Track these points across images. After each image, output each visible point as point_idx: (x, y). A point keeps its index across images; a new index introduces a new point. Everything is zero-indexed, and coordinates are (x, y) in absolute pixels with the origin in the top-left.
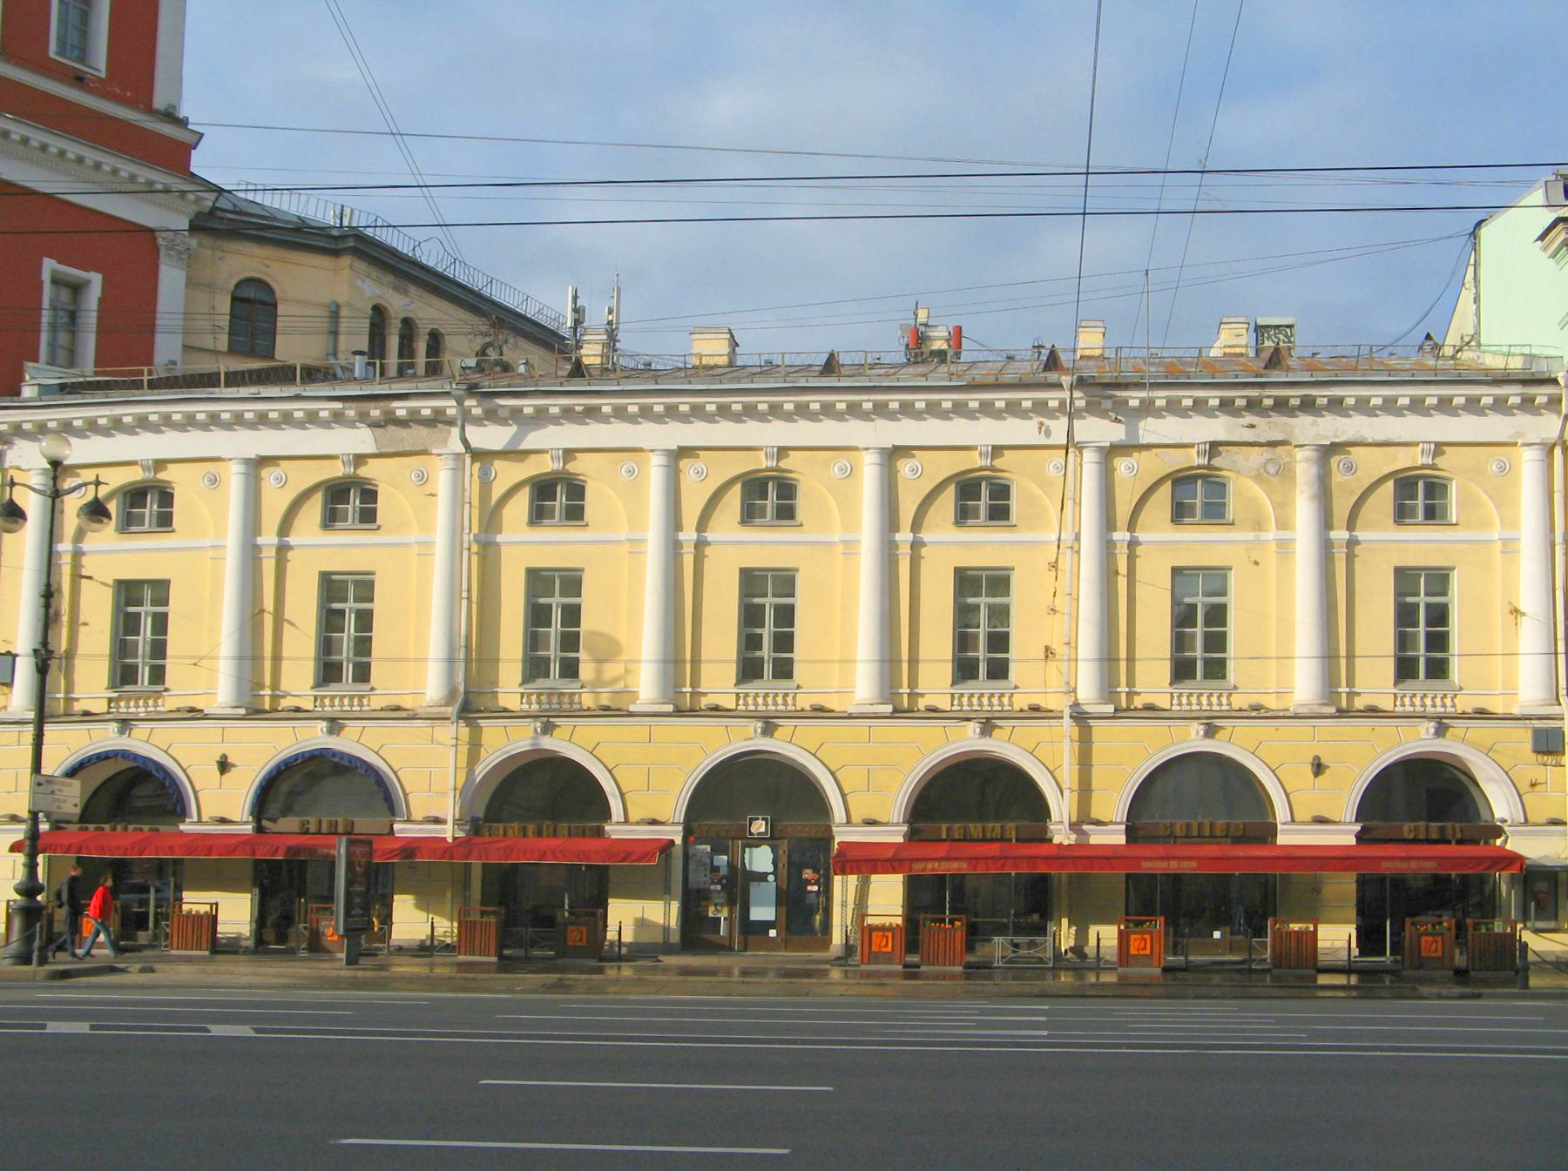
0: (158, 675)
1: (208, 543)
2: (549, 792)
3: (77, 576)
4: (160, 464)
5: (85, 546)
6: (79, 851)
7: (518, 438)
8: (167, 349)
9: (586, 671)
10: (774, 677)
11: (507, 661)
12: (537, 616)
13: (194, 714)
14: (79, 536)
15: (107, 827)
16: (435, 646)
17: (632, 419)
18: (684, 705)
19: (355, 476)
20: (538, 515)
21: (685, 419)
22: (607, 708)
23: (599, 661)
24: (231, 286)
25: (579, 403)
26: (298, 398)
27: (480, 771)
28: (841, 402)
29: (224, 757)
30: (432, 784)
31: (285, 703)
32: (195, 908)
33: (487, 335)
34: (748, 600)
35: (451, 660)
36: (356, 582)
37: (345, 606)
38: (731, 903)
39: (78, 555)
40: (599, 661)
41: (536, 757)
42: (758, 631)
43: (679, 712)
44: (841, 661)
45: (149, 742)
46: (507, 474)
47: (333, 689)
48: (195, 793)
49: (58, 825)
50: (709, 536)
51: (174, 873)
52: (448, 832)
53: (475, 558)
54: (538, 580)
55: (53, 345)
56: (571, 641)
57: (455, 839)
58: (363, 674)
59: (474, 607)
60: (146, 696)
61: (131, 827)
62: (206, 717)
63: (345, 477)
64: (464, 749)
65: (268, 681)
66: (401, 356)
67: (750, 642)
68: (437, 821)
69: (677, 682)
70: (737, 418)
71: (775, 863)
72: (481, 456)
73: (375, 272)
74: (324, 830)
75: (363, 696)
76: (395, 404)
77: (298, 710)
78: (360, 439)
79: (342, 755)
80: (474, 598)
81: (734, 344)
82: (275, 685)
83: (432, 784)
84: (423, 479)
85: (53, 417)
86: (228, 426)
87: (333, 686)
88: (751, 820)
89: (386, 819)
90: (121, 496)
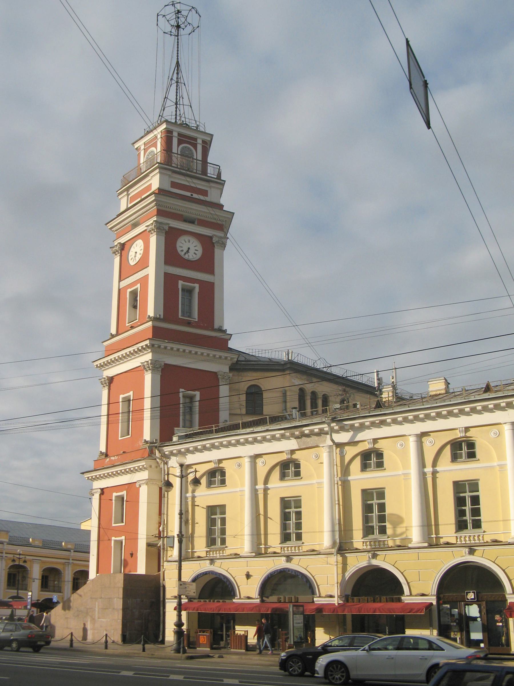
0: (223, 541)
1: (238, 489)
2: (376, 583)
3: (194, 506)
4: (220, 461)
5: (196, 494)
6: (197, 610)
7: (354, 436)
8: (224, 416)
9: (389, 531)
10: (473, 528)
11: (359, 530)
12: (367, 509)
13: (237, 556)
14: (193, 491)
15: (207, 600)
16: (326, 526)
17: (400, 423)
18: (433, 542)
19: (291, 458)
20: (365, 467)
21: (422, 420)
22: (399, 546)
23: (394, 528)
24: (245, 389)
25: (377, 419)
26: (267, 431)
27: (348, 575)
28: (491, 404)
29: (248, 572)
30: (329, 582)
31: (270, 550)
32: (239, 633)
33: (342, 395)
34: (458, 495)
35: (333, 531)
36: (294, 500)
37: (291, 509)
38: (461, 631)
39: (193, 497)
40: (394, 528)
41: (369, 569)
42: (464, 508)
43: (431, 546)
44: (503, 521)
45: (222, 568)
46: (350, 452)
47: (288, 544)
48: (238, 587)
49: (190, 599)
50: (438, 469)
51: (231, 619)
52: (336, 601)
53: (340, 487)
54: (366, 494)
55: (184, 420)
56: (382, 519)
57: (339, 604)
58: (299, 537)
59: (341, 507)
60: (220, 550)
61: (216, 600)
62: (241, 557)
63: (288, 459)
64: (340, 566)
65: (263, 542)
66: (239, 429)
67: (460, 513)
68: (331, 596)
69: (430, 533)
70: (445, 417)
71: (480, 612)
72: (339, 445)
73: (299, 375)
74: (287, 601)
75: (300, 546)
76: (304, 429)
77: (275, 553)
78: (292, 444)
79: (292, 570)
80: (341, 504)
81: (447, 384)
82: (266, 543)
83: (329, 582)
84: (318, 457)
85: (183, 447)
86: (243, 444)
87: (288, 542)
88: (467, 593)
89: (311, 596)
90: (207, 474)
